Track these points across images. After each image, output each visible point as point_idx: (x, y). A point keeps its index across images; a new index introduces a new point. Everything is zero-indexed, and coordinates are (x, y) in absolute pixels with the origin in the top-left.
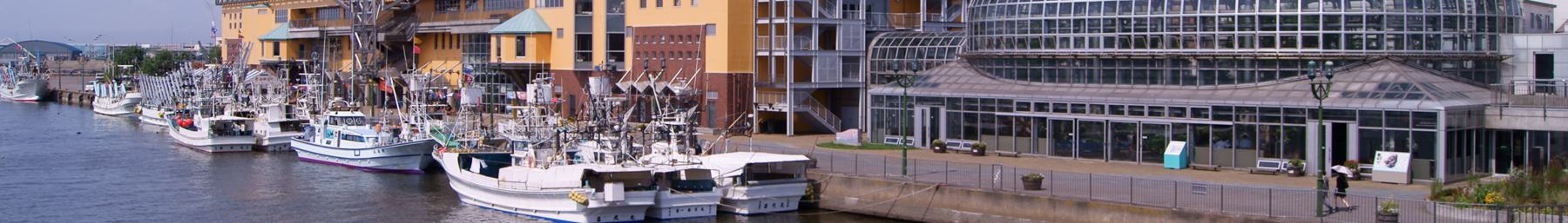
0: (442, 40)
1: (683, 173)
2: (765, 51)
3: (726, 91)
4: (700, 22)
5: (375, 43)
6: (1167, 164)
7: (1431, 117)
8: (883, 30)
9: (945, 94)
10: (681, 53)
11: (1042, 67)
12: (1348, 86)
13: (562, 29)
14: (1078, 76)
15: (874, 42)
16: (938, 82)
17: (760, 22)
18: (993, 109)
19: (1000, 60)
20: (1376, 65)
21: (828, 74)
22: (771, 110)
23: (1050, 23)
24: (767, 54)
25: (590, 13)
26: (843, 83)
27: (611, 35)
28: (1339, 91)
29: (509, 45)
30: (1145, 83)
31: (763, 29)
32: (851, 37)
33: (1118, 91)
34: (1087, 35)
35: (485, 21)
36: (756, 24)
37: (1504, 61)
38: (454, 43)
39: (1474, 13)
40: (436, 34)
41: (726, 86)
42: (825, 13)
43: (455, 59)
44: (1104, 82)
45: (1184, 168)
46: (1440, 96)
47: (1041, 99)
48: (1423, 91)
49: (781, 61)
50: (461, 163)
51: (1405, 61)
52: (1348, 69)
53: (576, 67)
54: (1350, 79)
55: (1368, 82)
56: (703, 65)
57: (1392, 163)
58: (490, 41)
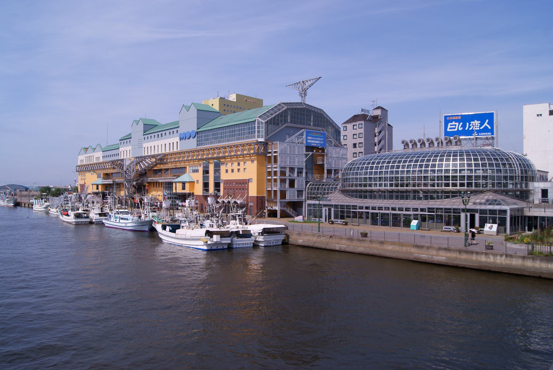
0: (156, 184)
1: (241, 231)
4: (247, 178)
5: (132, 185)
6: (412, 228)
7: (505, 211)
8: (311, 181)
9: (333, 203)
11: (368, 194)
12: (475, 201)
13: (198, 180)
15: (308, 185)
17: (268, 178)
18: (350, 209)
19: (353, 191)
20: (485, 193)
22: (272, 209)
23: (370, 178)
24: (271, 189)
25: (208, 175)
29: (179, 186)
31: (269, 180)
33: (394, 202)
39: (520, 175)
42: (291, 175)
43: (160, 191)
46: (508, 204)
47: (367, 205)
49: (275, 192)
51: (496, 192)
52: (475, 195)
54: (476, 198)
57: (491, 228)
58: (173, 184)
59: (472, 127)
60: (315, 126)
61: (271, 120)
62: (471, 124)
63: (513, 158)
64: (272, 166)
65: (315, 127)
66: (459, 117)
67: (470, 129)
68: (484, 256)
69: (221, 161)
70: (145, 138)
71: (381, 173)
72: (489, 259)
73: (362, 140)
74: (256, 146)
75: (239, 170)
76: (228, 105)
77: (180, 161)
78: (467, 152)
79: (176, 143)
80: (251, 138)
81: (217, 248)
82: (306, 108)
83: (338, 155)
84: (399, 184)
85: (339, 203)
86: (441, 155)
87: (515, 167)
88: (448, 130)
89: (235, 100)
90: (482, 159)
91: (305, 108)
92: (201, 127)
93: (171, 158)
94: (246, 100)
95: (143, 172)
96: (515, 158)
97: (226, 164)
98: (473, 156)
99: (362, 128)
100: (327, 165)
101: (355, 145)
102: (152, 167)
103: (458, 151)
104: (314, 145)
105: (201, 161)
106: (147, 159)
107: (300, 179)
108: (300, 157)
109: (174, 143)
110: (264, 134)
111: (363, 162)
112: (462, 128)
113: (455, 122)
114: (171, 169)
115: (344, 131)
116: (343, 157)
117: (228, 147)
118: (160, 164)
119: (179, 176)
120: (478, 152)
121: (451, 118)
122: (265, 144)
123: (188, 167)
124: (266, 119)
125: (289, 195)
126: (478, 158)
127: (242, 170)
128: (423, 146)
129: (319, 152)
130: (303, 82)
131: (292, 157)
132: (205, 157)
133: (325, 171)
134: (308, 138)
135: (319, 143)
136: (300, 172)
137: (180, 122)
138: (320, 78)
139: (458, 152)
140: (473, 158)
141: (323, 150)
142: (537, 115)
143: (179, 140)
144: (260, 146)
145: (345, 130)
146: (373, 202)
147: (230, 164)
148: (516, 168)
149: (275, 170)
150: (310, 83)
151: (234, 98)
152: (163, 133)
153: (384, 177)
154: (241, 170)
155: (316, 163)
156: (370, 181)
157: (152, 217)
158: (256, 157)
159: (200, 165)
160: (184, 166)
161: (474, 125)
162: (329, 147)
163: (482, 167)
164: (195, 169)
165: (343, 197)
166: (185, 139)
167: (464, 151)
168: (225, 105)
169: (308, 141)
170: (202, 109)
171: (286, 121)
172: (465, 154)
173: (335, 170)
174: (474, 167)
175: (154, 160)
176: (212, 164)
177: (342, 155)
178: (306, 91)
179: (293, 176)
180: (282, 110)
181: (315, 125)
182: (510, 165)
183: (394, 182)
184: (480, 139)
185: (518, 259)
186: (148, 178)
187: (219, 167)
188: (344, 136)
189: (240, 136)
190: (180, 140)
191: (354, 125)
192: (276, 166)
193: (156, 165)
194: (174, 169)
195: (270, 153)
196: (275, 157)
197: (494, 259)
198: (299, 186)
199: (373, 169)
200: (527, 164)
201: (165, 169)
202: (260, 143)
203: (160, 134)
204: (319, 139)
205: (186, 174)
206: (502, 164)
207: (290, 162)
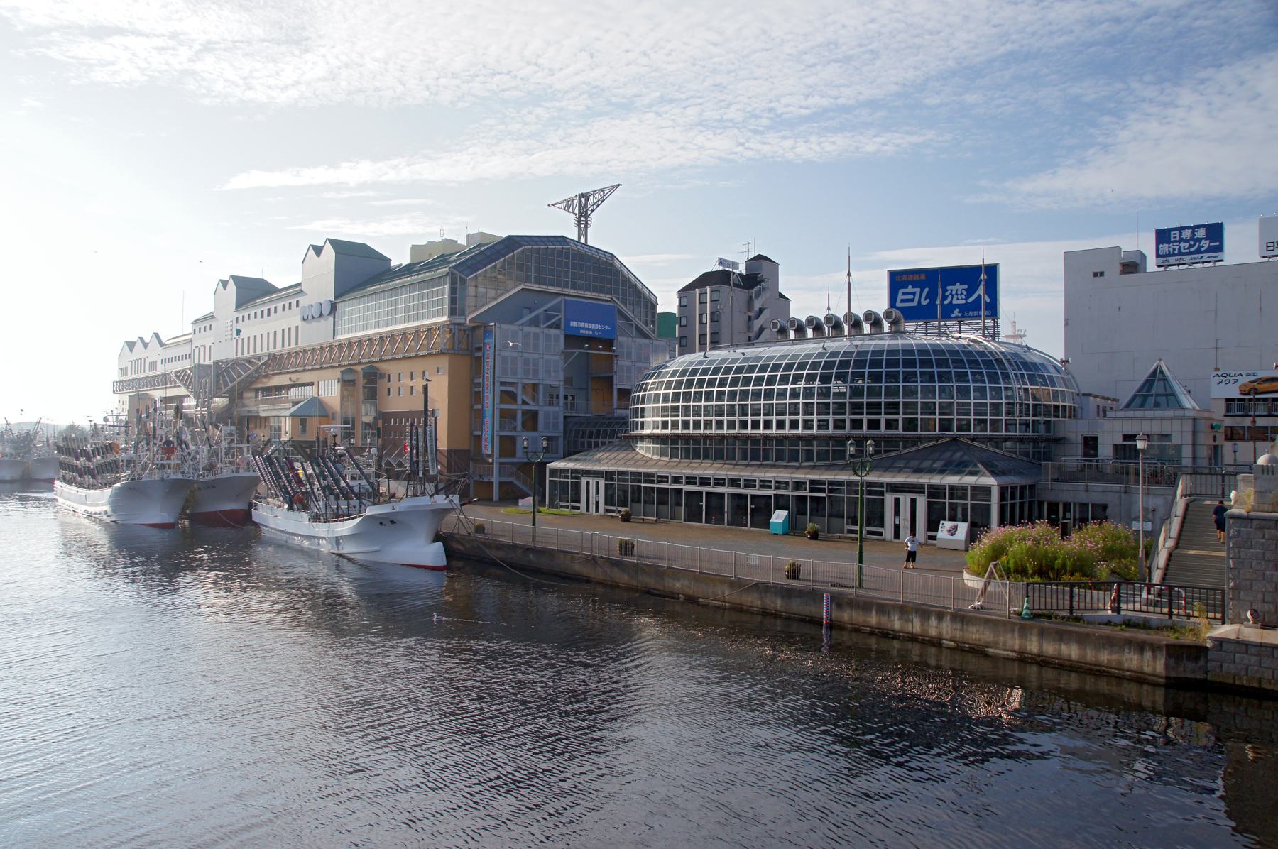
6: (772, 530)
7: (987, 490)
9: (605, 468)
12: (920, 464)
14: (719, 456)
22: (180, 476)
34: (725, 418)
45: (787, 534)
57: (953, 531)
59: (950, 297)
65: (601, 295)
67: (946, 302)
68: (897, 617)
72: (910, 625)
102: (252, 383)
104: (587, 332)
112: (928, 300)
121: (905, 278)
135: (598, 330)
141: (609, 343)
150: (559, 206)
161: (954, 293)
185: (982, 628)
197: (922, 625)
202: (456, 327)
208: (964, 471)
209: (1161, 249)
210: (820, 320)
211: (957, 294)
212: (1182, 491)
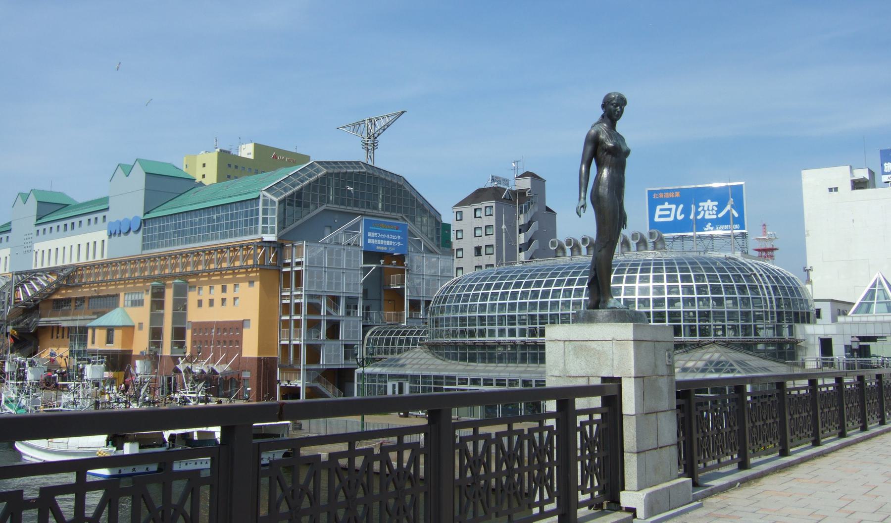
0: (56, 331)
1: (195, 434)
2: (286, 340)
3: (256, 371)
5: (5, 333)
8: (377, 324)
9: (409, 372)
10: (225, 342)
11: (477, 351)
12: (686, 363)
13: (142, 323)
14: (512, 359)
15: (369, 333)
16: (406, 363)
17: (284, 318)
19: (448, 345)
20: (706, 348)
21: (333, 358)
22: (289, 385)
23: (482, 319)
24: (287, 342)
25: (162, 311)
26: (345, 364)
27: (175, 327)
28: (679, 368)
29: (101, 335)
30: (516, 363)
31: (286, 324)
32: (351, 329)
33: (529, 369)
35: (86, 317)
36: (281, 320)
37: (799, 344)
38: (66, 334)
39: (775, 309)
40: (53, 326)
41: (256, 367)
42: (331, 311)
43: (65, 346)
44: (489, 362)
47: (474, 375)
48: (736, 367)
49: (297, 347)
50: (683, 462)
51: (727, 344)
52: (687, 351)
53: (171, 354)
54: (687, 359)
55: (700, 360)
56: (241, 354)
58: (87, 332)
60: (387, 210)
61: (292, 195)
62: (700, 206)
63: (761, 275)
64: (291, 293)
65: (393, 214)
66: (676, 193)
67: (699, 217)
69: (189, 283)
70: (38, 231)
71: (543, 306)
73: (492, 240)
74: (259, 251)
75: (224, 300)
76: (236, 167)
77: (107, 282)
78: (669, 263)
79: (86, 245)
80: (251, 234)
81: (134, 472)
82: (368, 173)
83: (433, 271)
84: (538, 330)
85: (420, 372)
86: (617, 269)
87: (764, 294)
88: (657, 219)
89: (252, 157)
90: (698, 278)
91: (364, 173)
92: (154, 209)
93: (89, 275)
94: (275, 157)
95: (30, 305)
96: (764, 276)
97: (199, 288)
98: (680, 272)
99: (492, 215)
100: (410, 291)
101: (478, 251)
102: (50, 295)
103: (652, 262)
104: (382, 248)
105: (170, 280)
106: (39, 275)
107: (350, 321)
108: (352, 275)
109: (97, 243)
110: (276, 225)
111: (476, 284)
112: (683, 216)
113: (669, 204)
114: (90, 298)
115: (457, 220)
116: (445, 274)
117: (216, 250)
118: (67, 287)
119: (103, 313)
120: (691, 263)
121: (661, 195)
122: (279, 247)
123: (122, 295)
124: (282, 194)
125: (326, 355)
126: (690, 275)
127: (230, 301)
128: (576, 253)
129: (392, 264)
130: (370, 120)
131: (334, 274)
132: (178, 270)
133: (406, 304)
134: (370, 234)
135: (392, 246)
136: (351, 305)
137: (110, 199)
138: (403, 112)
139: (652, 264)
140: (681, 276)
141: (401, 259)
142: (828, 190)
143: (107, 236)
144: (268, 251)
145: (458, 218)
146: (487, 368)
147: (206, 288)
148: (767, 296)
149: (297, 301)
150: (383, 123)
151: (249, 152)
152: (76, 221)
153: (519, 315)
154: (227, 302)
155: (387, 287)
156: (481, 325)
157: (5, 402)
158: (258, 274)
159: (147, 291)
160: (114, 293)
161: (706, 209)
162: (415, 254)
163: (698, 294)
164: (137, 298)
165: (429, 359)
166: (120, 234)
167: (664, 262)
168: (230, 165)
169: (369, 241)
170: (152, 172)
171: (325, 200)
172: (664, 267)
173: (348, 299)
174: (698, 294)
175: (53, 278)
176: (171, 288)
177: (442, 271)
178: (376, 138)
179: (336, 315)
180: (316, 177)
181: (386, 208)
182: (754, 288)
183: (527, 327)
184: (688, 238)
186: (40, 317)
187: (185, 294)
188: (457, 231)
189: (231, 229)
190: (110, 235)
191: (476, 210)
192: (299, 293)
193: (57, 291)
194: (105, 299)
195: (288, 265)
196: (299, 273)
198: (349, 336)
199: (538, 296)
200: (790, 288)
201: (77, 299)
202: (267, 244)
203: (69, 222)
204: (393, 237)
205: (118, 310)
206: (737, 288)
207: (330, 284)
208: (722, 369)
209: (885, 167)
210: (593, 239)
211: (708, 210)
212: (259, 202)
